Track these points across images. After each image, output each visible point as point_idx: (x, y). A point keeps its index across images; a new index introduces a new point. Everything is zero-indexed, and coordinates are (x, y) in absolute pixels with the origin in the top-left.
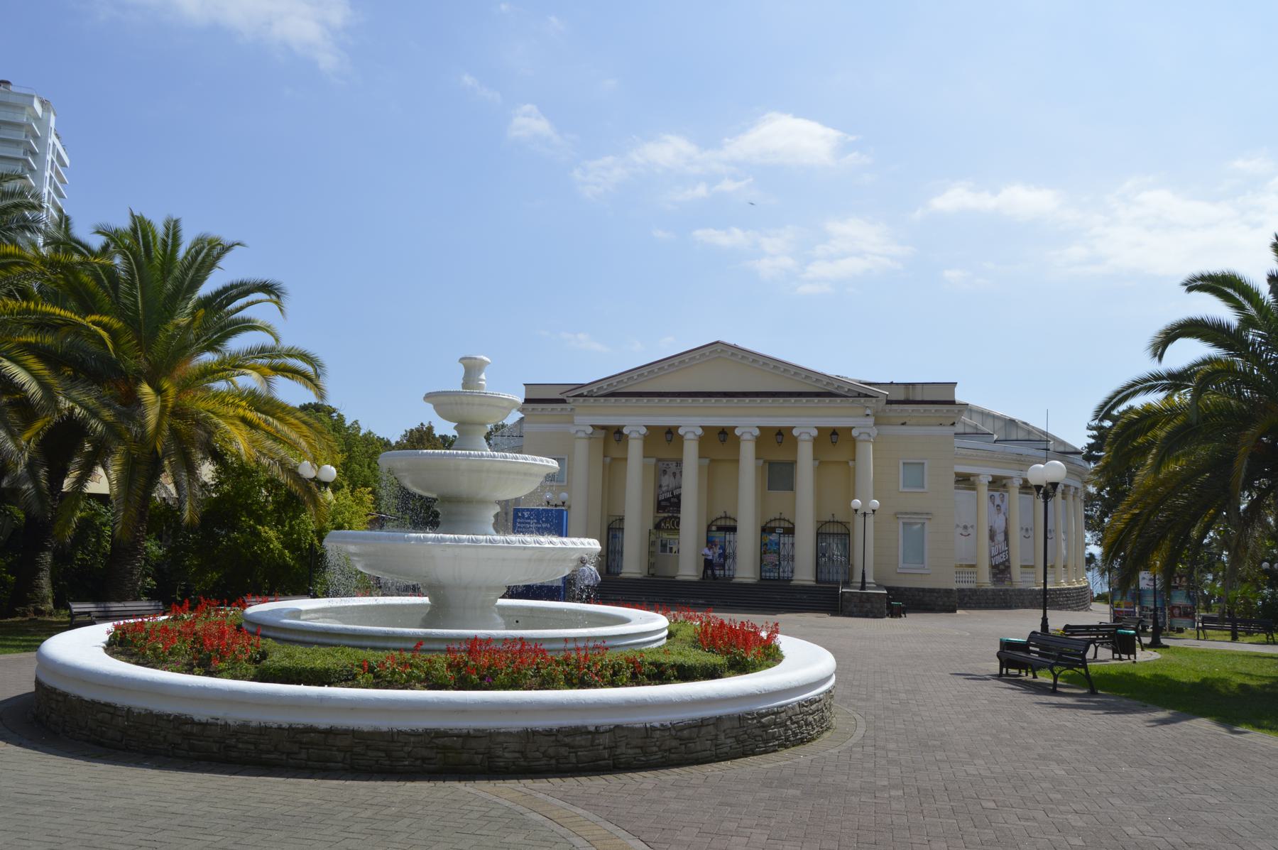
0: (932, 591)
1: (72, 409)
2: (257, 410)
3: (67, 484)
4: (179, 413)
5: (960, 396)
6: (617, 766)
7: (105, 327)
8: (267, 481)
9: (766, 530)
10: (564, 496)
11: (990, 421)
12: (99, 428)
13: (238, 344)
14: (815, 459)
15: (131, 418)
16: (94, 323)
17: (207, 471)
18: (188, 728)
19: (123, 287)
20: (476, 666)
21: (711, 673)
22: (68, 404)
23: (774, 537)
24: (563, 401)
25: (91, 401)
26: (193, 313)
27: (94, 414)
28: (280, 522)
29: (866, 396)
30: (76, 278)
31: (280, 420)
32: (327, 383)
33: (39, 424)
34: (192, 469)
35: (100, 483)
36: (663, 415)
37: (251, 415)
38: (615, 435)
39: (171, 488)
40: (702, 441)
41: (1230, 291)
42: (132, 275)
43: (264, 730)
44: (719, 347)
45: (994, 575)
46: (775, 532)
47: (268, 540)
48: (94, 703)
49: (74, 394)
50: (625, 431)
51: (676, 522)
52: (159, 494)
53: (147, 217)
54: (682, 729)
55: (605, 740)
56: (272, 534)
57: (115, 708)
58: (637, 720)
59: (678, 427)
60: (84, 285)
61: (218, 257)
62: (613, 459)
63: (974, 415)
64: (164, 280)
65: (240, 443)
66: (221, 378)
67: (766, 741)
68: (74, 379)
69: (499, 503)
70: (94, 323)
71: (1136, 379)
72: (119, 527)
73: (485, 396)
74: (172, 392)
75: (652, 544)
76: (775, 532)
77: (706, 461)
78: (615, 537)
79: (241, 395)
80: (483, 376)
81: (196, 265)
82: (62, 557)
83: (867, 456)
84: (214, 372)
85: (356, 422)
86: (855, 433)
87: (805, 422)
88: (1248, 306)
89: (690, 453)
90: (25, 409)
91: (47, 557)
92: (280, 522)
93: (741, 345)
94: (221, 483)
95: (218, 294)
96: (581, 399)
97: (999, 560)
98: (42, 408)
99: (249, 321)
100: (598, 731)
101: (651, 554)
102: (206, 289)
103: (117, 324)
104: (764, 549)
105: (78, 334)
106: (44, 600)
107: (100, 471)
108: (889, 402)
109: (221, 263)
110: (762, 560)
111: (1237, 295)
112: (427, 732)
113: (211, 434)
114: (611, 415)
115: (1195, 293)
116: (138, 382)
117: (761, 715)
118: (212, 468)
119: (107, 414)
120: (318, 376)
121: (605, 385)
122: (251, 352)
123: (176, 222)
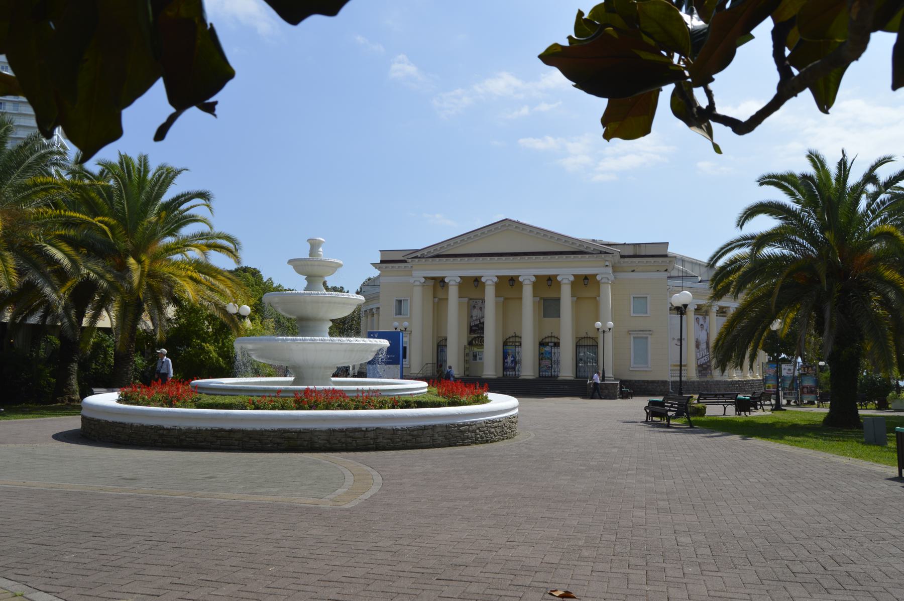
0: (653, 382)
1: (88, 274)
2: (199, 272)
3: (85, 322)
4: (152, 275)
5: (671, 250)
6: (378, 448)
7: (106, 224)
8: (208, 316)
9: (542, 344)
10: (406, 324)
11: (697, 268)
12: (105, 285)
13: (187, 231)
14: (572, 296)
15: (124, 279)
16: (100, 222)
17: (171, 311)
18: (161, 432)
19: (116, 199)
20: (304, 400)
21: (439, 405)
22: (86, 271)
23: (547, 349)
24: (404, 261)
25: (99, 269)
26: (158, 214)
27: (102, 277)
28: (216, 341)
29: (606, 253)
30: (87, 194)
31: (214, 277)
32: (242, 254)
33: (69, 284)
34: (161, 309)
35: (105, 321)
36: (471, 269)
37: (195, 275)
38: (440, 283)
39: (149, 323)
40: (535, 285)
41: (786, 184)
42: (121, 191)
43: (199, 431)
44: (507, 223)
45: (700, 371)
46: (547, 346)
47: (209, 352)
48: (114, 423)
49: (89, 265)
50: (446, 280)
51: (481, 339)
52: (141, 327)
53: (129, 155)
54: (413, 430)
55: (372, 435)
56: (211, 348)
57: (125, 424)
58: (389, 425)
59: (481, 277)
60: (92, 198)
61: (173, 178)
62: (440, 299)
63: (686, 264)
64: (140, 194)
65: (190, 292)
66: (177, 253)
67: (463, 440)
68: (88, 255)
69: (332, 320)
70: (100, 222)
71: (733, 240)
72: (118, 344)
73: (321, 261)
74: (147, 262)
75: (467, 355)
76: (547, 346)
77: (502, 299)
78: (442, 351)
79: (190, 264)
80: (321, 249)
81: (159, 184)
82: (83, 367)
83: (607, 293)
84: (173, 249)
85: (270, 279)
86: (598, 278)
87: (565, 271)
88: (797, 193)
89: (490, 293)
90: (62, 275)
91: (75, 367)
92: (216, 341)
93: (521, 221)
94: (179, 318)
95: (174, 200)
96: (417, 260)
97: (702, 361)
98: (72, 274)
99: (193, 216)
100: (367, 430)
101: (466, 361)
102: (167, 197)
103: (113, 222)
104: (541, 357)
105: (90, 229)
106: (74, 393)
107: (104, 313)
108: (623, 257)
109: (175, 181)
110: (540, 364)
111: (790, 187)
112: (279, 430)
113: (172, 287)
114: (437, 270)
115: (765, 186)
116: (126, 256)
117: (459, 426)
118: (174, 309)
119: (109, 276)
120: (237, 250)
121: (432, 250)
122: (194, 236)
123: (145, 157)
